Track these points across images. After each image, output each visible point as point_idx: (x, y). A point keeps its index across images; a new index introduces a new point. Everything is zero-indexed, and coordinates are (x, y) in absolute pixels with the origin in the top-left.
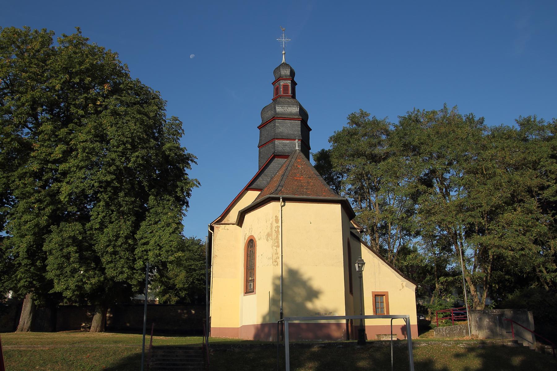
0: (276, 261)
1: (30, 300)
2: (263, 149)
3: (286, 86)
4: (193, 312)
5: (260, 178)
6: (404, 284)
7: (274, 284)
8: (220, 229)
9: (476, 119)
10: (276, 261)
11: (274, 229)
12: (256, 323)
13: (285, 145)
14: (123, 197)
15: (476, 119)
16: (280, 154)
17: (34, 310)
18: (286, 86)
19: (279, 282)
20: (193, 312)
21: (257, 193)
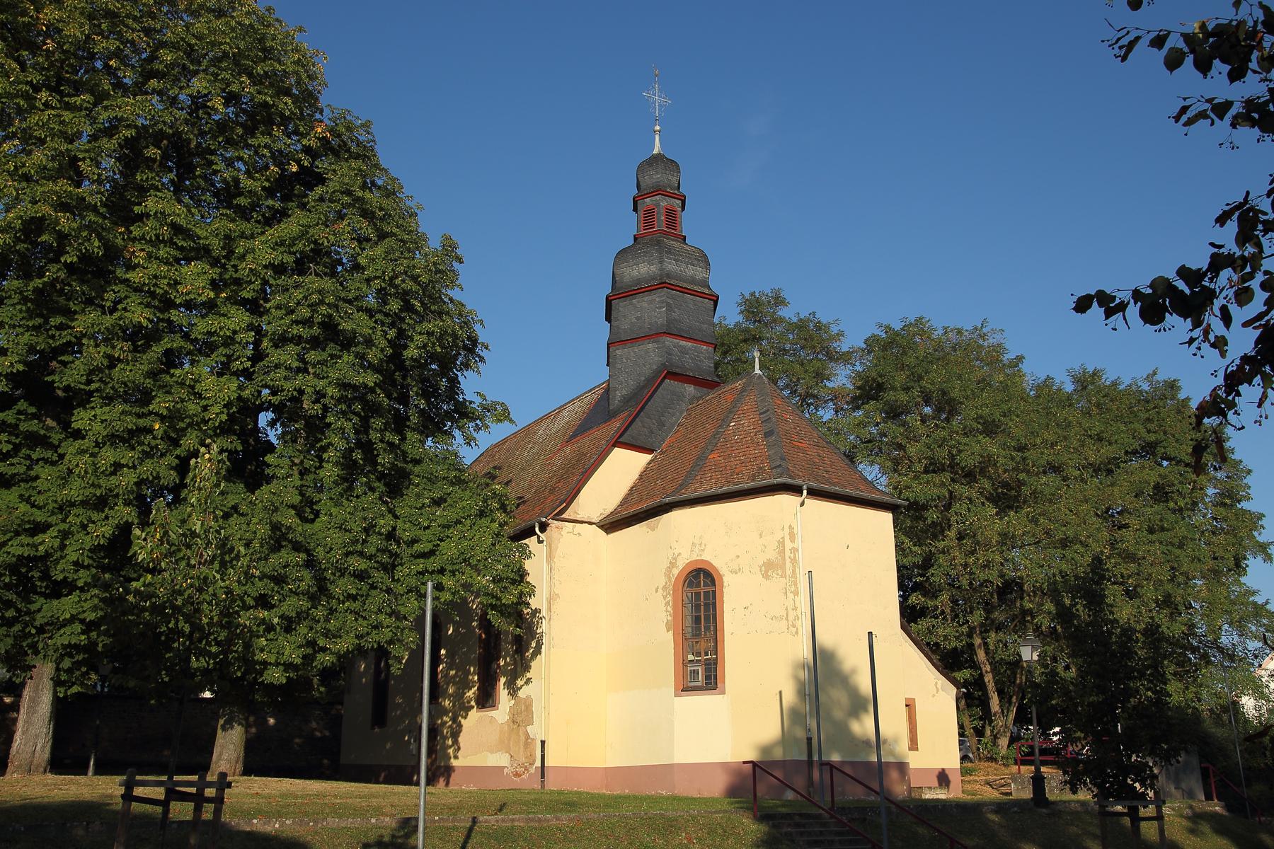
0: (794, 626)
1: (48, 684)
2: (619, 352)
3: (658, 205)
4: (272, 721)
5: (638, 422)
6: (939, 682)
7: (796, 678)
8: (564, 532)
9: (1006, 357)
10: (794, 626)
11: (788, 554)
12: (728, 759)
13: (684, 351)
14: (382, 431)
15: (1006, 357)
16: (678, 370)
17: (63, 712)
18: (658, 205)
19: (804, 675)
20: (272, 721)
21: (642, 459)
